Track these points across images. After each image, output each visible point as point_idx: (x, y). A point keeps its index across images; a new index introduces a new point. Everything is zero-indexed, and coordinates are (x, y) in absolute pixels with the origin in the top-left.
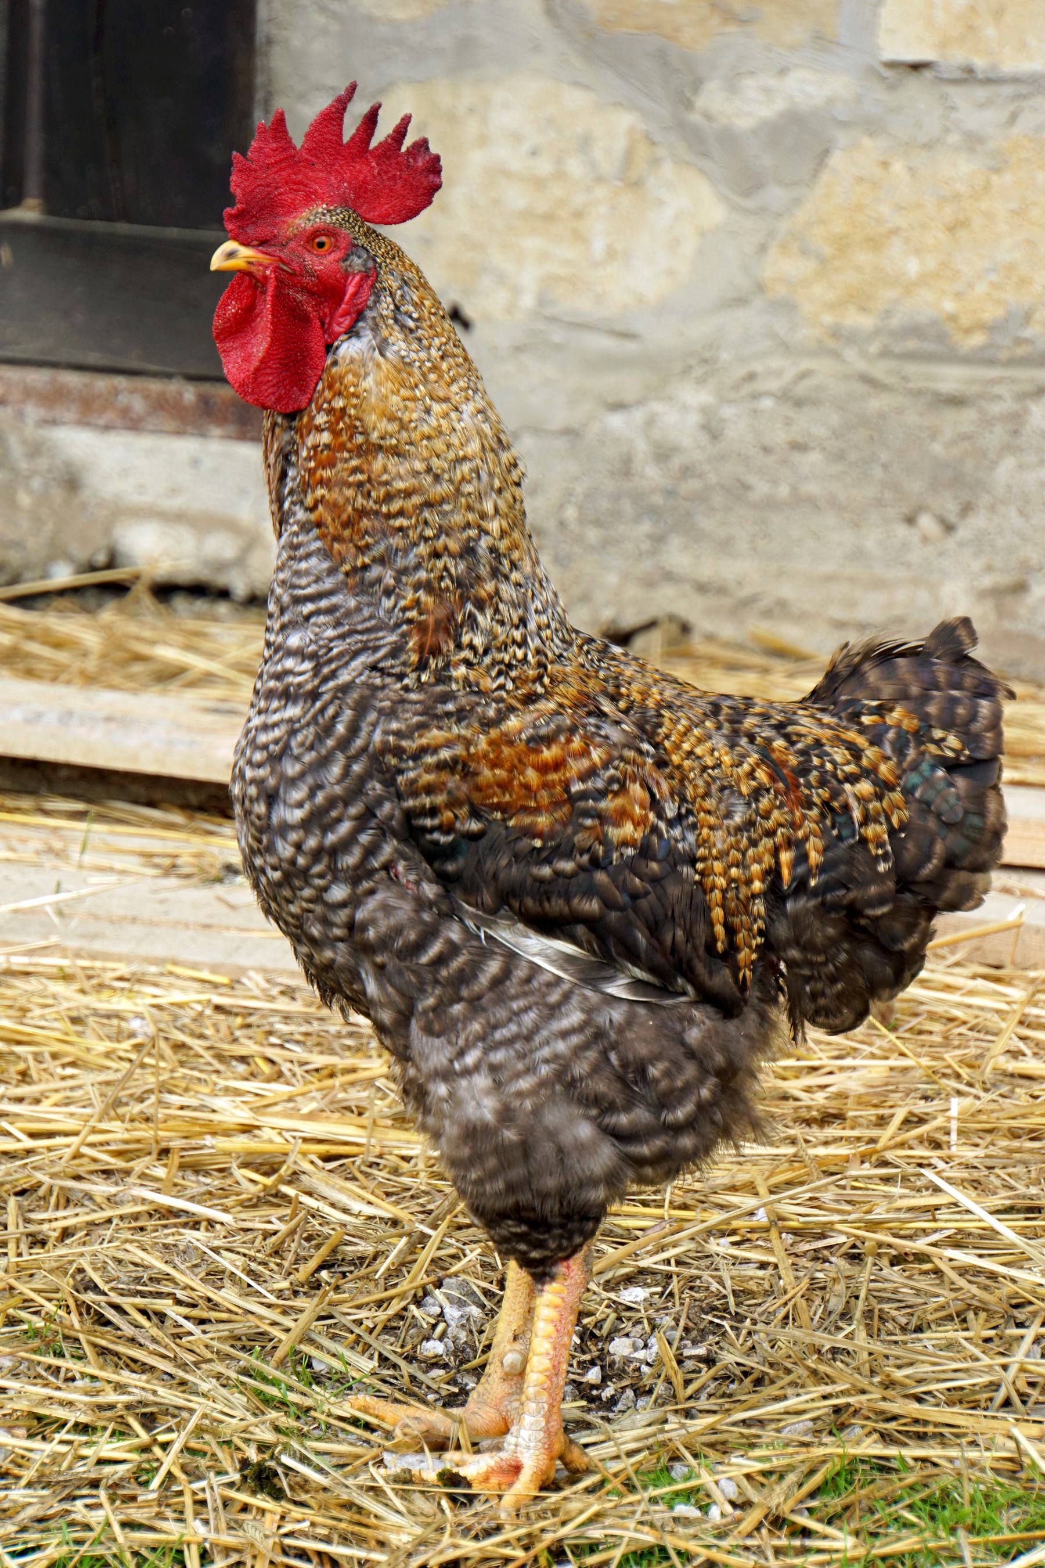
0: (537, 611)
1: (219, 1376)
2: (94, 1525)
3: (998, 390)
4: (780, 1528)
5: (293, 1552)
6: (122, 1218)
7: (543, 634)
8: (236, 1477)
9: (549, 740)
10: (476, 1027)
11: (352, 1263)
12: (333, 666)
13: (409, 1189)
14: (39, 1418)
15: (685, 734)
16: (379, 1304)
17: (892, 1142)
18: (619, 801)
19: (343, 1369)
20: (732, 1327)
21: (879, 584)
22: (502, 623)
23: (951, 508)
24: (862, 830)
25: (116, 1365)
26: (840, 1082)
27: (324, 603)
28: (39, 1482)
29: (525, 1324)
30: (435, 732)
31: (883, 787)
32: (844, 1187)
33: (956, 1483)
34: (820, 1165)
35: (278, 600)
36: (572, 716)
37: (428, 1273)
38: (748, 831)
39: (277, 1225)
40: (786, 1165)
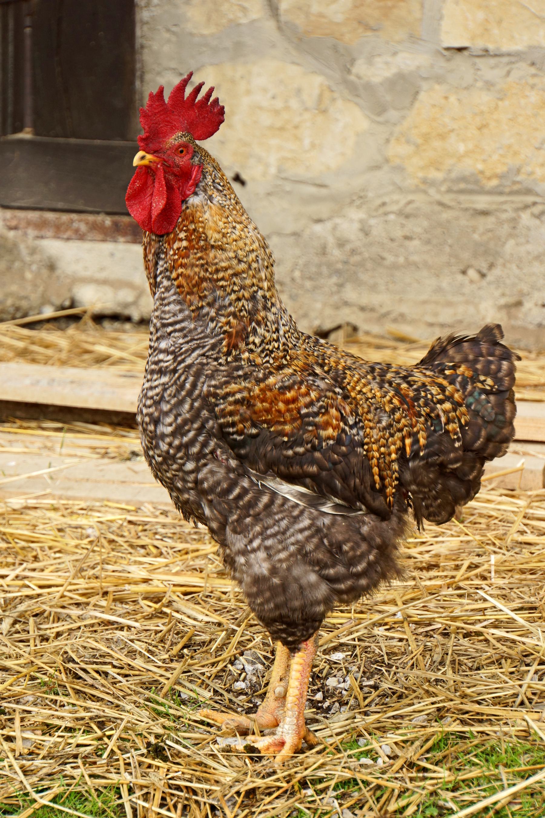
0: (283, 325)
1: (135, 702)
2: (76, 776)
3: (505, 207)
4: (412, 768)
5: (174, 787)
6: (85, 626)
7: (287, 335)
8: (145, 751)
9: (289, 388)
10: (258, 528)
11: (199, 645)
12: (183, 357)
13: (226, 608)
14: (48, 725)
15: (357, 382)
16: (213, 664)
17: (463, 578)
18: (325, 418)
19: (196, 697)
20: (386, 671)
21: (449, 304)
22: (268, 331)
23: (484, 267)
24: (446, 427)
25: (85, 698)
26: (436, 549)
27: (178, 327)
28: (48, 756)
29: (286, 673)
30: (233, 385)
31: (457, 405)
32: (439, 600)
33: (498, 743)
34: (428, 590)
35: (155, 325)
36: (301, 376)
37: (236, 649)
38: (389, 429)
39: (162, 628)
40: (411, 590)
